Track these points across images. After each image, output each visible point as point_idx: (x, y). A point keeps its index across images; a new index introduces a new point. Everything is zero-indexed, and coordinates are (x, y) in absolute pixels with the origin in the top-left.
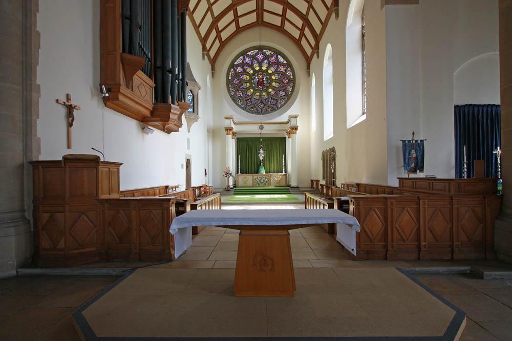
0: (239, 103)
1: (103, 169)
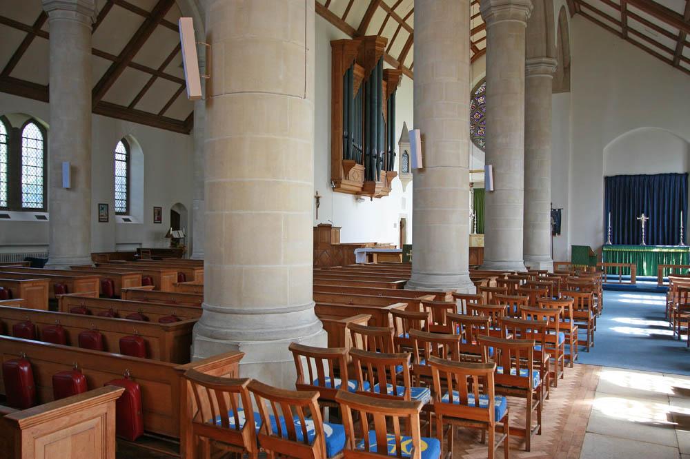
1: (333, 230)
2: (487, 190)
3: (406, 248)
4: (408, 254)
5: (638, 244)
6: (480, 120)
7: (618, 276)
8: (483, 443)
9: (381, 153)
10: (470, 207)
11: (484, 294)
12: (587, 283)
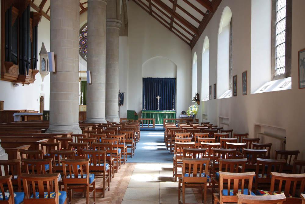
0: (85, 57)
2: (88, 82)
3: (46, 113)
4: (46, 116)
5: (156, 109)
6: (85, 45)
7: (147, 124)
8: (85, 197)
9: (29, 59)
10: (79, 91)
11: (86, 134)
12: (132, 127)
